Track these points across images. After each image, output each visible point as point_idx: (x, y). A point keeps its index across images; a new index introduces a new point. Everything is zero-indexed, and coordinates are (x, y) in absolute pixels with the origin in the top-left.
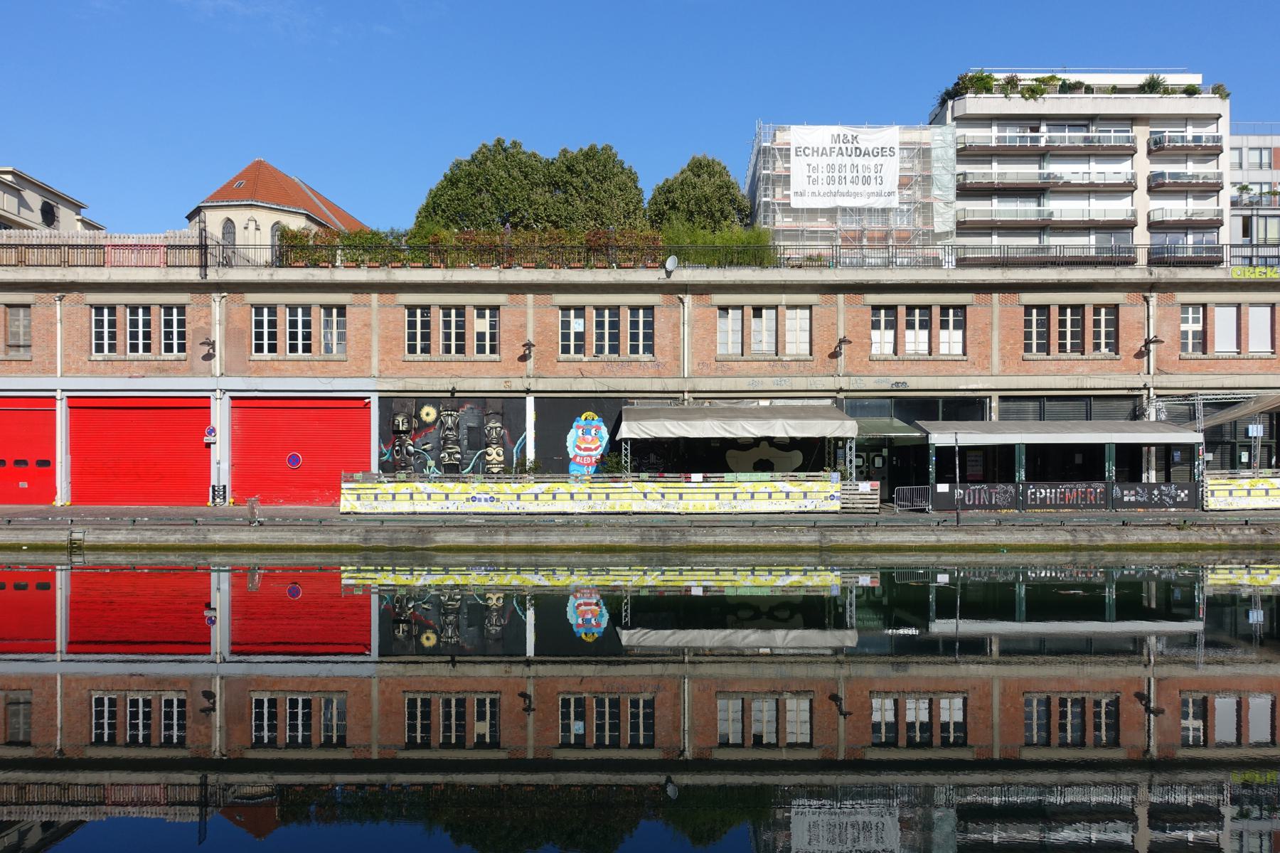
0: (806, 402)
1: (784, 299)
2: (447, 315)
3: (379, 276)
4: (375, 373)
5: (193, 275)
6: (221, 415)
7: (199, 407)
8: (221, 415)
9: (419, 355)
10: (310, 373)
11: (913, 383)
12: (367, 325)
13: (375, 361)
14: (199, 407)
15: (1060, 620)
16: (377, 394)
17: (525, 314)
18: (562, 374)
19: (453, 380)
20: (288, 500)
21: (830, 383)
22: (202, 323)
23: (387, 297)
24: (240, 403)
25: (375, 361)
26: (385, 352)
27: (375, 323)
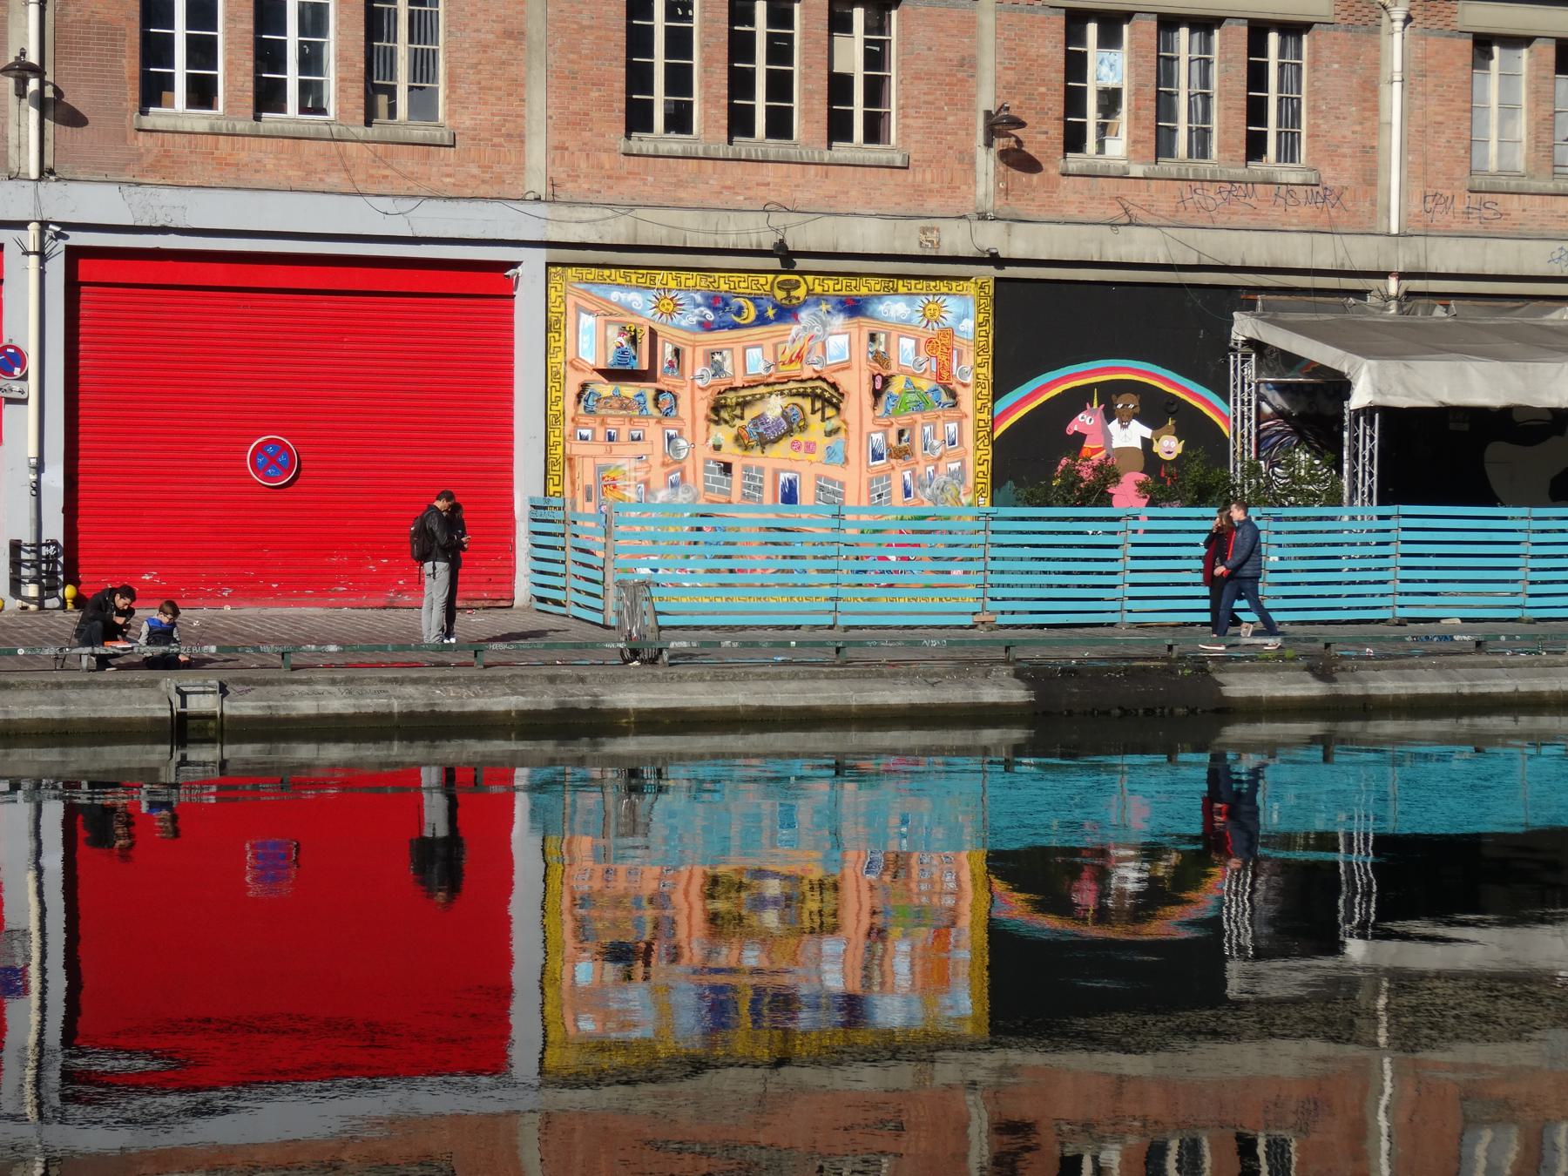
4: (538, 185)
10: (335, 179)
12: (515, 35)
13: (536, 152)
16: (542, 255)
19: (778, 219)
25: (536, 152)
26: (568, 122)
27: (536, 28)
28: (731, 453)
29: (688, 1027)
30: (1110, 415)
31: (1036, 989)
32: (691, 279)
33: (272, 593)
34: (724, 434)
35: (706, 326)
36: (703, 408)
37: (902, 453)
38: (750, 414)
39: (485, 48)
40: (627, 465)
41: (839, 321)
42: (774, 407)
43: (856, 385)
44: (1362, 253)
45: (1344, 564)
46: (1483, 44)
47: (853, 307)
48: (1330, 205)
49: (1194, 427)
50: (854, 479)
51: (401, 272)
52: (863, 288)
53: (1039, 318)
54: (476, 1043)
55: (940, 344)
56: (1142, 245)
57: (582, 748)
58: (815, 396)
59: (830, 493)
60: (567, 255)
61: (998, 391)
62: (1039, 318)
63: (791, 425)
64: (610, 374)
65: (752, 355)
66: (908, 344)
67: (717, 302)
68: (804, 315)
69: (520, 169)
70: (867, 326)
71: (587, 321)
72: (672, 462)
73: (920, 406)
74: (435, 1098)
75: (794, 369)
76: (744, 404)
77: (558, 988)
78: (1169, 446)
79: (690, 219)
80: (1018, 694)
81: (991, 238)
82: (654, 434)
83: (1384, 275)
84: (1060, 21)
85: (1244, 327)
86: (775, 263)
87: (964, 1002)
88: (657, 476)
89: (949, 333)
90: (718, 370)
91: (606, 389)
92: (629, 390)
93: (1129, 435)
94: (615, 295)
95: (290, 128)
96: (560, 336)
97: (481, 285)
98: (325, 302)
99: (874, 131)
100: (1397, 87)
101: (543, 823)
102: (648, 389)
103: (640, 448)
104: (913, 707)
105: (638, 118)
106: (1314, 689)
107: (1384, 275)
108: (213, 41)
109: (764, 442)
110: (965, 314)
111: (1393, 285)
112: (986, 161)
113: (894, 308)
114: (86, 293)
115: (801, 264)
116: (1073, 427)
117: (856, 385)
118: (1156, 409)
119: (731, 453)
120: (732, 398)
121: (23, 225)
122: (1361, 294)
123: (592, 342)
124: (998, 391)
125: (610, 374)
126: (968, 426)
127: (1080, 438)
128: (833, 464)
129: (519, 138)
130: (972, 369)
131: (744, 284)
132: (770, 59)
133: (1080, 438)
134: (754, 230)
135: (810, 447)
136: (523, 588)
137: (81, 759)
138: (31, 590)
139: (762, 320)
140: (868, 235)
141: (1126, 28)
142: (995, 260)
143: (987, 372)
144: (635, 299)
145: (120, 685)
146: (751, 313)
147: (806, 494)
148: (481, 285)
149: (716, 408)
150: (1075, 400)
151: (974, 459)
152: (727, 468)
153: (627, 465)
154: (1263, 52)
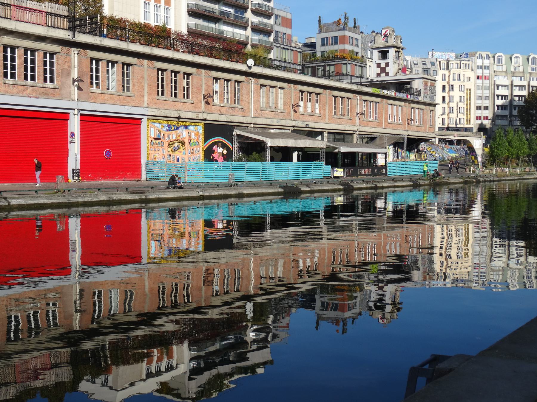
0: (283, 131)
1: (279, 84)
2: (45, 56)
3: (146, 50)
4: (146, 105)
5: (63, 34)
6: (74, 125)
7: (62, 118)
8: (74, 125)
9: (48, 84)
10: (118, 103)
11: (312, 125)
12: (142, 77)
13: (146, 98)
14: (62, 118)
15: (140, 247)
16: (146, 117)
17: (201, 79)
18: (214, 112)
19: (179, 112)
20: (104, 178)
21: (290, 123)
22: (66, 66)
23: (151, 62)
24: (87, 119)
25: (146, 98)
26: (150, 94)
27: (146, 77)
28: (171, 153)
29: (166, 254)
30: (218, 147)
31: (211, 245)
32: (165, 122)
33: (107, 178)
34: (170, 149)
35: (168, 130)
36: (167, 145)
37: (192, 153)
38: (173, 146)
39: (138, 79)
40: (157, 155)
41: (184, 130)
42: (176, 145)
43: (187, 141)
44: (249, 120)
45: (268, 171)
46: (262, 85)
47: (186, 127)
48: (245, 112)
49: (228, 149)
50: (186, 157)
51: (117, 119)
52: (188, 124)
53: (212, 130)
54: (136, 259)
55: (197, 134)
56: (223, 118)
57: (241, 200)
58: (182, 143)
59: (183, 160)
60: (153, 118)
61: (205, 142)
62: (212, 130)
63: (179, 148)
64: (155, 139)
65: (173, 136)
66: (193, 134)
67: (169, 126)
68: (180, 129)
69: (144, 101)
70: (188, 131)
71: (152, 129)
72: (163, 155)
73: (195, 145)
74: (51, 283)
75: (178, 138)
76: (172, 144)
77: (149, 248)
78: (225, 152)
79: (167, 112)
80: (281, 190)
81: (205, 116)
82: (161, 149)
83: (251, 124)
84: (89, 60)
85: (236, 132)
86: (177, 119)
87: (200, 248)
88: (161, 157)
89: (198, 132)
90: (169, 139)
91: (154, 141)
92: (157, 141)
93: (220, 150)
94: (156, 125)
95: (29, 84)
96: (148, 131)
97: (137, 122)
98: (114, 125)
99: (52, 81)
100: (76, 69)
101: (147, 218)
102: (160, 141)
103: (159, 152)
104: (273, 192)
105: (5, 75)
106: (308, 189)
107: (251, 124)
108: (15, 65)
109: (175, 151)
110: (200, 129)
111: (252, 125)
112: (203, 103)
113: (191, 128)
114: (342, 136)
115: (180, 120)
116: (213, 149)
117: (187, 141)
118: (224, 146)
119: (171, 153)
120: (171, 143)
121: (74, 109)
122: (247, 127)
123: (153, 133)
124: (205, 142)
125: (155, 139)
126: (201, 148)
127: (214, 150)
128: (182, 154)
129: (143, 96)
130: (201, 138)
131: (172, 123)
132: (11, 61)
133: (214, 150)
134: (175, 114)
135: (181, 152)
136: (144, 177)
137: (88, 210)
138: (77, 178)
139: (174, 130)
140: (190, 115)
141: (16, 50)
142: (205, 120)
143: (203, 139)
144: (158, 125)
145: (177, 191)
146: (173, 128)
147: (180, 160)
148: (137, 122)
149: (169, 145)
150: (213, 144)
151: (201, 154)
152: (170, 156)
153: (157, 155)
154: (7, 53)
